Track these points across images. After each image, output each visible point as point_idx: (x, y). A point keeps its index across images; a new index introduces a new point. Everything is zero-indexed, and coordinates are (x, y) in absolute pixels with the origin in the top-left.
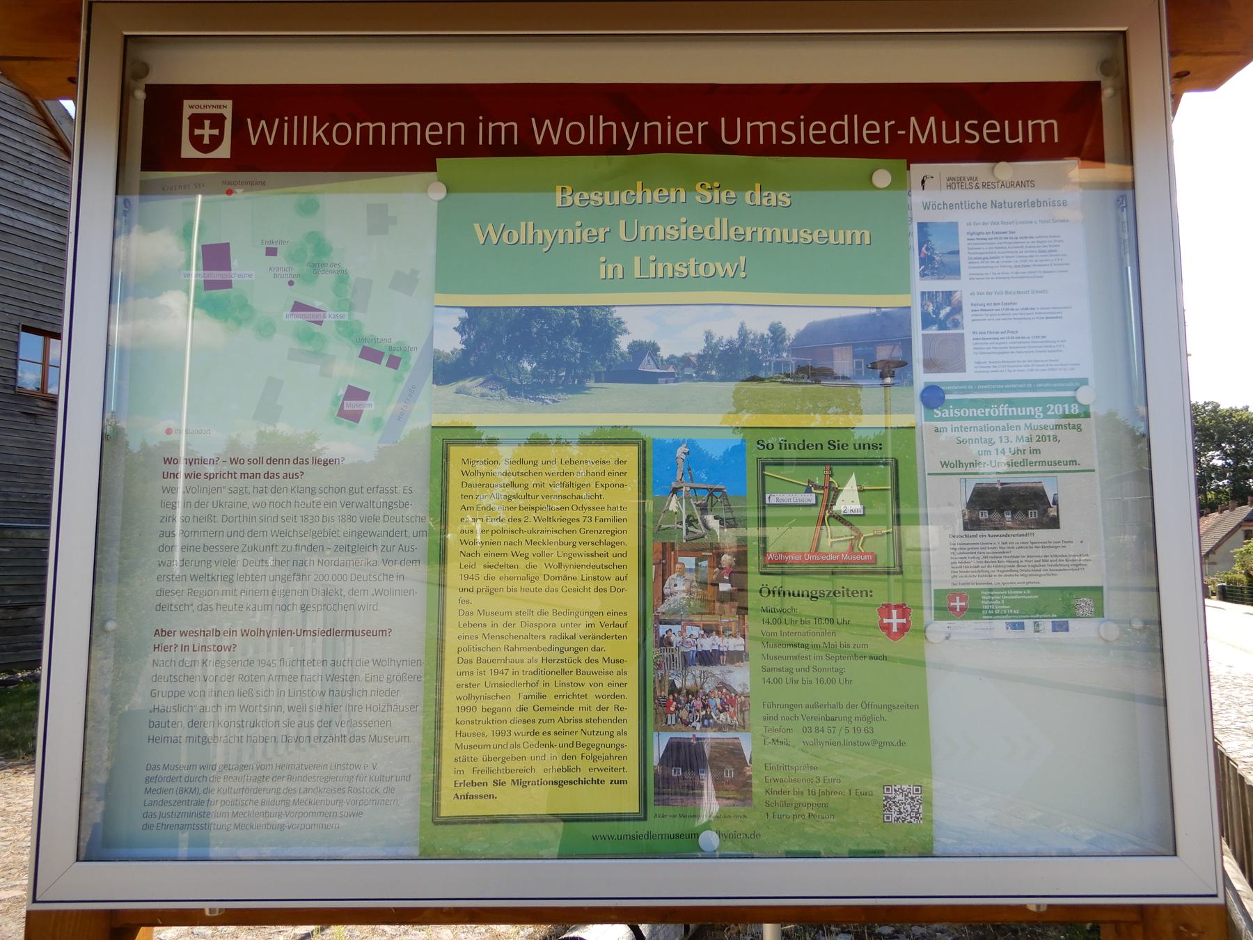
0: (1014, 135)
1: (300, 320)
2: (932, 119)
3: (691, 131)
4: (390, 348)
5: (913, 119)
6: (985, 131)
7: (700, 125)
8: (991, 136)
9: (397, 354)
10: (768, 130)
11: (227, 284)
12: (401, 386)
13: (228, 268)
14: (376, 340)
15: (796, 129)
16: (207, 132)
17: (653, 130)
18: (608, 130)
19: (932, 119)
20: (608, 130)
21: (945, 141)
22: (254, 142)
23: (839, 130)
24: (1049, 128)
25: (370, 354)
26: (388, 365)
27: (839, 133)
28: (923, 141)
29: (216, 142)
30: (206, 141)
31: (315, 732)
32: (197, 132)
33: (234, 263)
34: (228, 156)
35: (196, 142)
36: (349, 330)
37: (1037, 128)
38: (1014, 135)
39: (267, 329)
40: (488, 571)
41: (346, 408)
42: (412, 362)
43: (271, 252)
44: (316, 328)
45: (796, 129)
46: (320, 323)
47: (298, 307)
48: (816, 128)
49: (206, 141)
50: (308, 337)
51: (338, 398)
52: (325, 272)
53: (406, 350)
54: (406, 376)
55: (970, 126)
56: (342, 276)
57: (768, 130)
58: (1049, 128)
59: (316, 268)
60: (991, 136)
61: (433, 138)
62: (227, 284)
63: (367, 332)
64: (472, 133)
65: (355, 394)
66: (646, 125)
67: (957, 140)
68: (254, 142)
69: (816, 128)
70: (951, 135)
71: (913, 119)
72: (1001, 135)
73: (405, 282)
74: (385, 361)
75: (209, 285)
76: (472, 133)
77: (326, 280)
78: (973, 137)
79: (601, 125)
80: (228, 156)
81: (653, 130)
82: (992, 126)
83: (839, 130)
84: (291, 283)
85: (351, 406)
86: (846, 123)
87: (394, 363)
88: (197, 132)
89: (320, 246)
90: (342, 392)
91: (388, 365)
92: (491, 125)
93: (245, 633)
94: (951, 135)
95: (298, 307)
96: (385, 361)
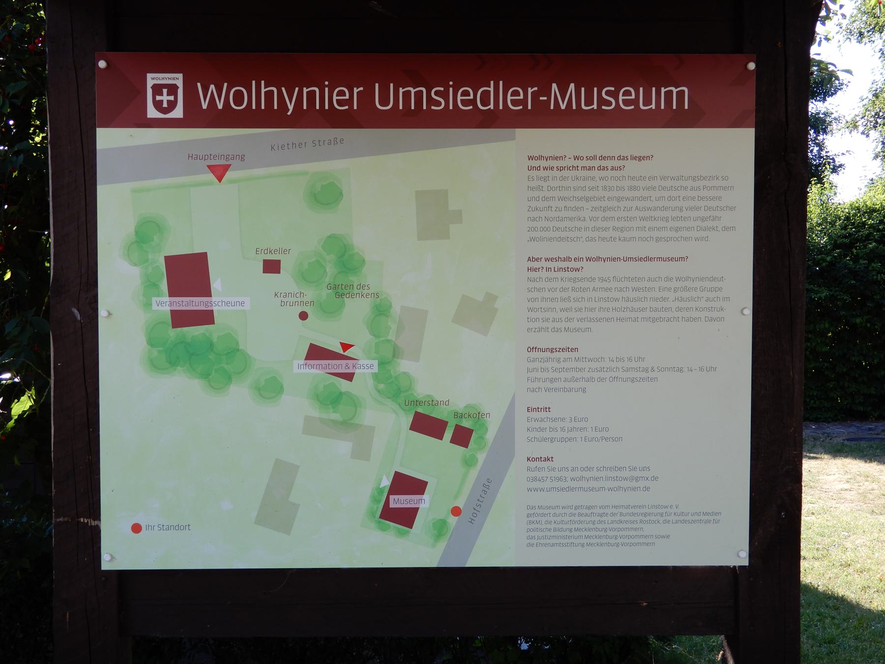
0: (647, 102)
1: (317, 372)
2: (572, 86)
3: (521, 97)
4: (456, 415)
5: (554, 86)
6: (621, 98)
7: (356, 90)
8: (626, 102)
9: (466, 424)
10: (419, 95)
11: (206, 318)
12: (474, 473)
13: (208, 294)
14: (433, 403)
15: (446, 98)
16: (165, 98)
17: (311, 95)
18: (269, 94)
19: (572, 86)
20: (269, 94)
21: (584, 107)
22: (205, 106)
23: (486, 94)
24: (681, 94)
25: (427, 425)
26: (453, 441)
28: (563, 107)
29: (172, 105)
30: (165, 105)
32: (158, 98)
33: (216, 284)
35: (158, 105)
36: (394, 388)
38: (647, 102)
39: (270, 389)
41: (392, 505)
42: (490, 436)
43: (272, 267)
44: (343, 384)
45: (446, 98)
46: (349, 377)
47: (316, 353)
49: (165, 105)
50: (333, 400)
51: (381, 491)
52: (352, 296)
53: (479, 416)
54: (481, 457)
55: (607, 93)
56: (381, 310)
57: (419, 95)
58: (681, 94)
59: (340, 291)
60: (626, 102)
61: (514, 103)
62: (206, 318)
63: (421, 390)
64: (366, 98)
65: (406, 484)
66: (305, 90)
67: (595, 106)
68: (205, 106)
70: (589, 102)
71: (554, 86)
72: (635, 102)
73: (476, 313)
74: (448, 434)
75: (180, 319)
76: (366, 98)
77: (357, 309)
78: (610, 104)
79: (263, 90)
81: (311, 95)
82: (627, 93)
83: (486, 94)
84: (303, 316)
85: (400, 501)
86: (492, 89)
87: (462, 437)
88: (158, 98)
89: (346, 259)
90: (386, 482)
91: (453, 441)
92: (401, 90)
94: (589, 102)
95: (316, 353)
96: (448, 434)
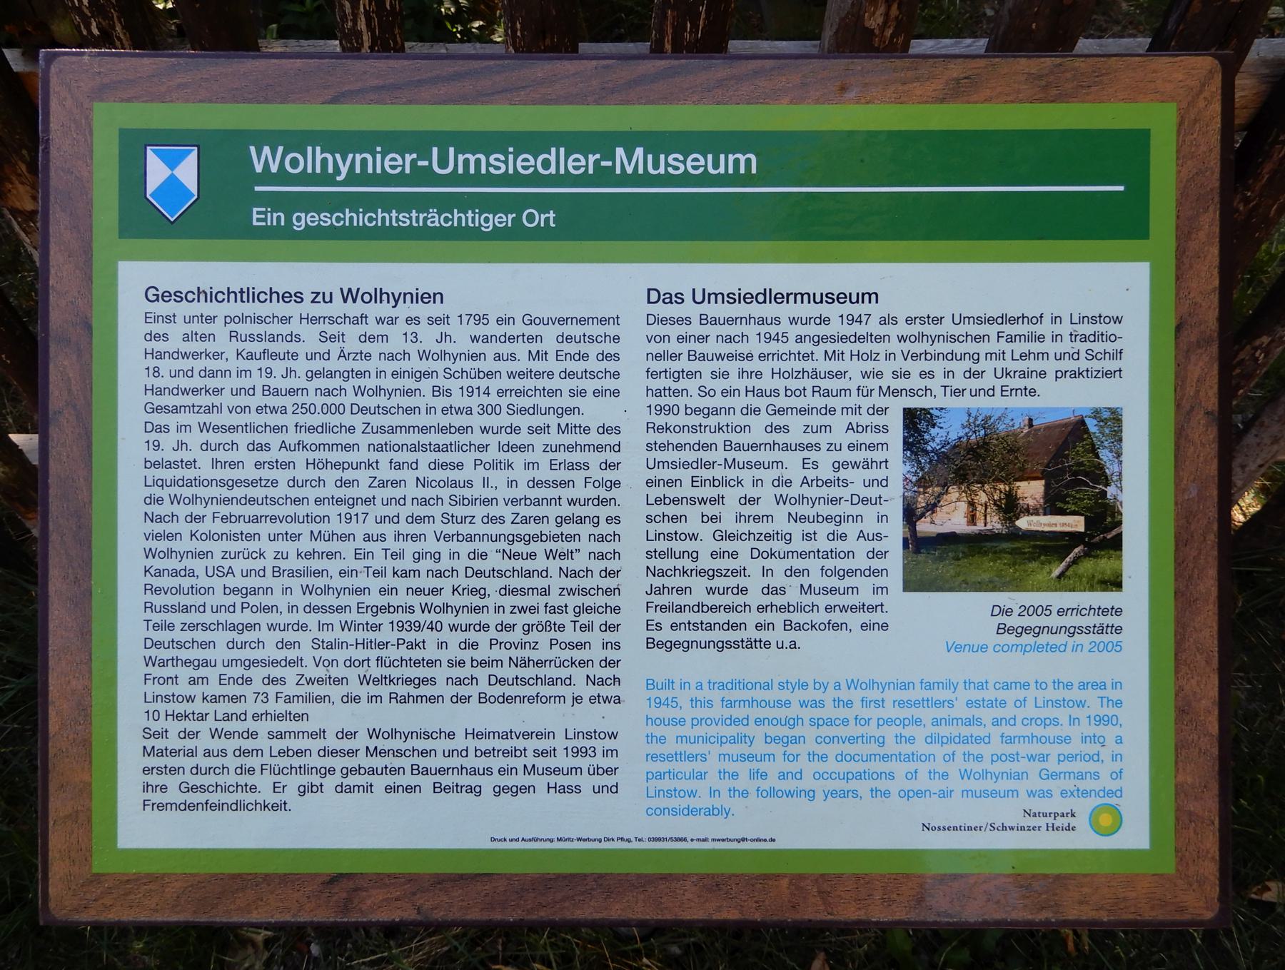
0: (716, 166)
10: (478, 162)
18: (324, 161)
20: (324, 161)
24: (748, 161)
26: (1082, 422)
27: (546, 164)
31: (831, 693)
34: (1148, 264)
37: (737, 161)
38: (716, 166)
40: (242, 760)
48: (575, 160)
57: (478, 162)
58: (748, 161)
69: (575, 160)
70: (656, 166)
80: (1148, 264)
81: (364, 161)
93: (983, 648)
94: (656, 166)
